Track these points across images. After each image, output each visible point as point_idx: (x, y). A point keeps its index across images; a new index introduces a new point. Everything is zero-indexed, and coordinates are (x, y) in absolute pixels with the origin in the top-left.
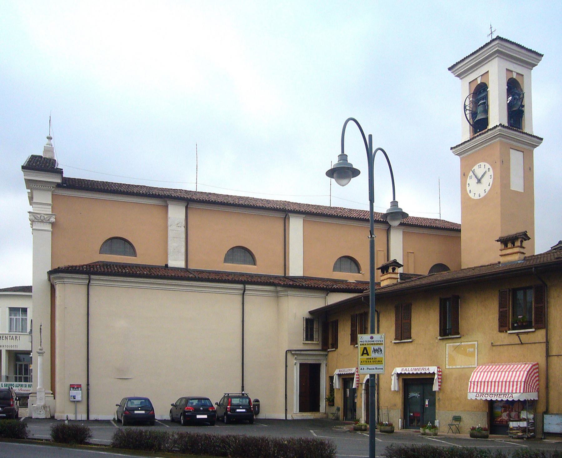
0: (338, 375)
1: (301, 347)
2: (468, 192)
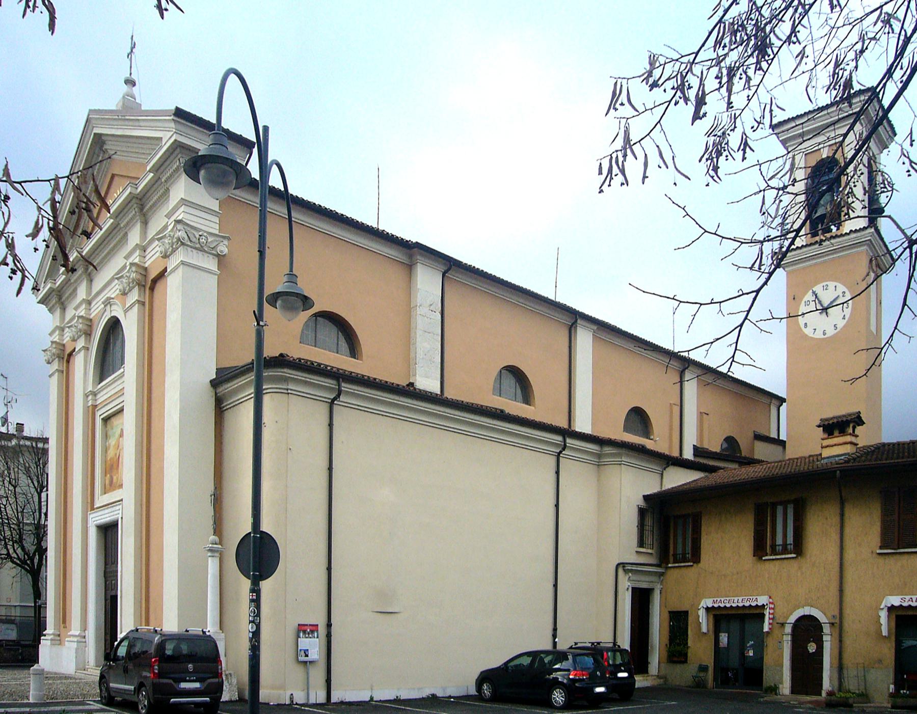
0: (706, 609)
1: (634, 559)
2: (802, 326)
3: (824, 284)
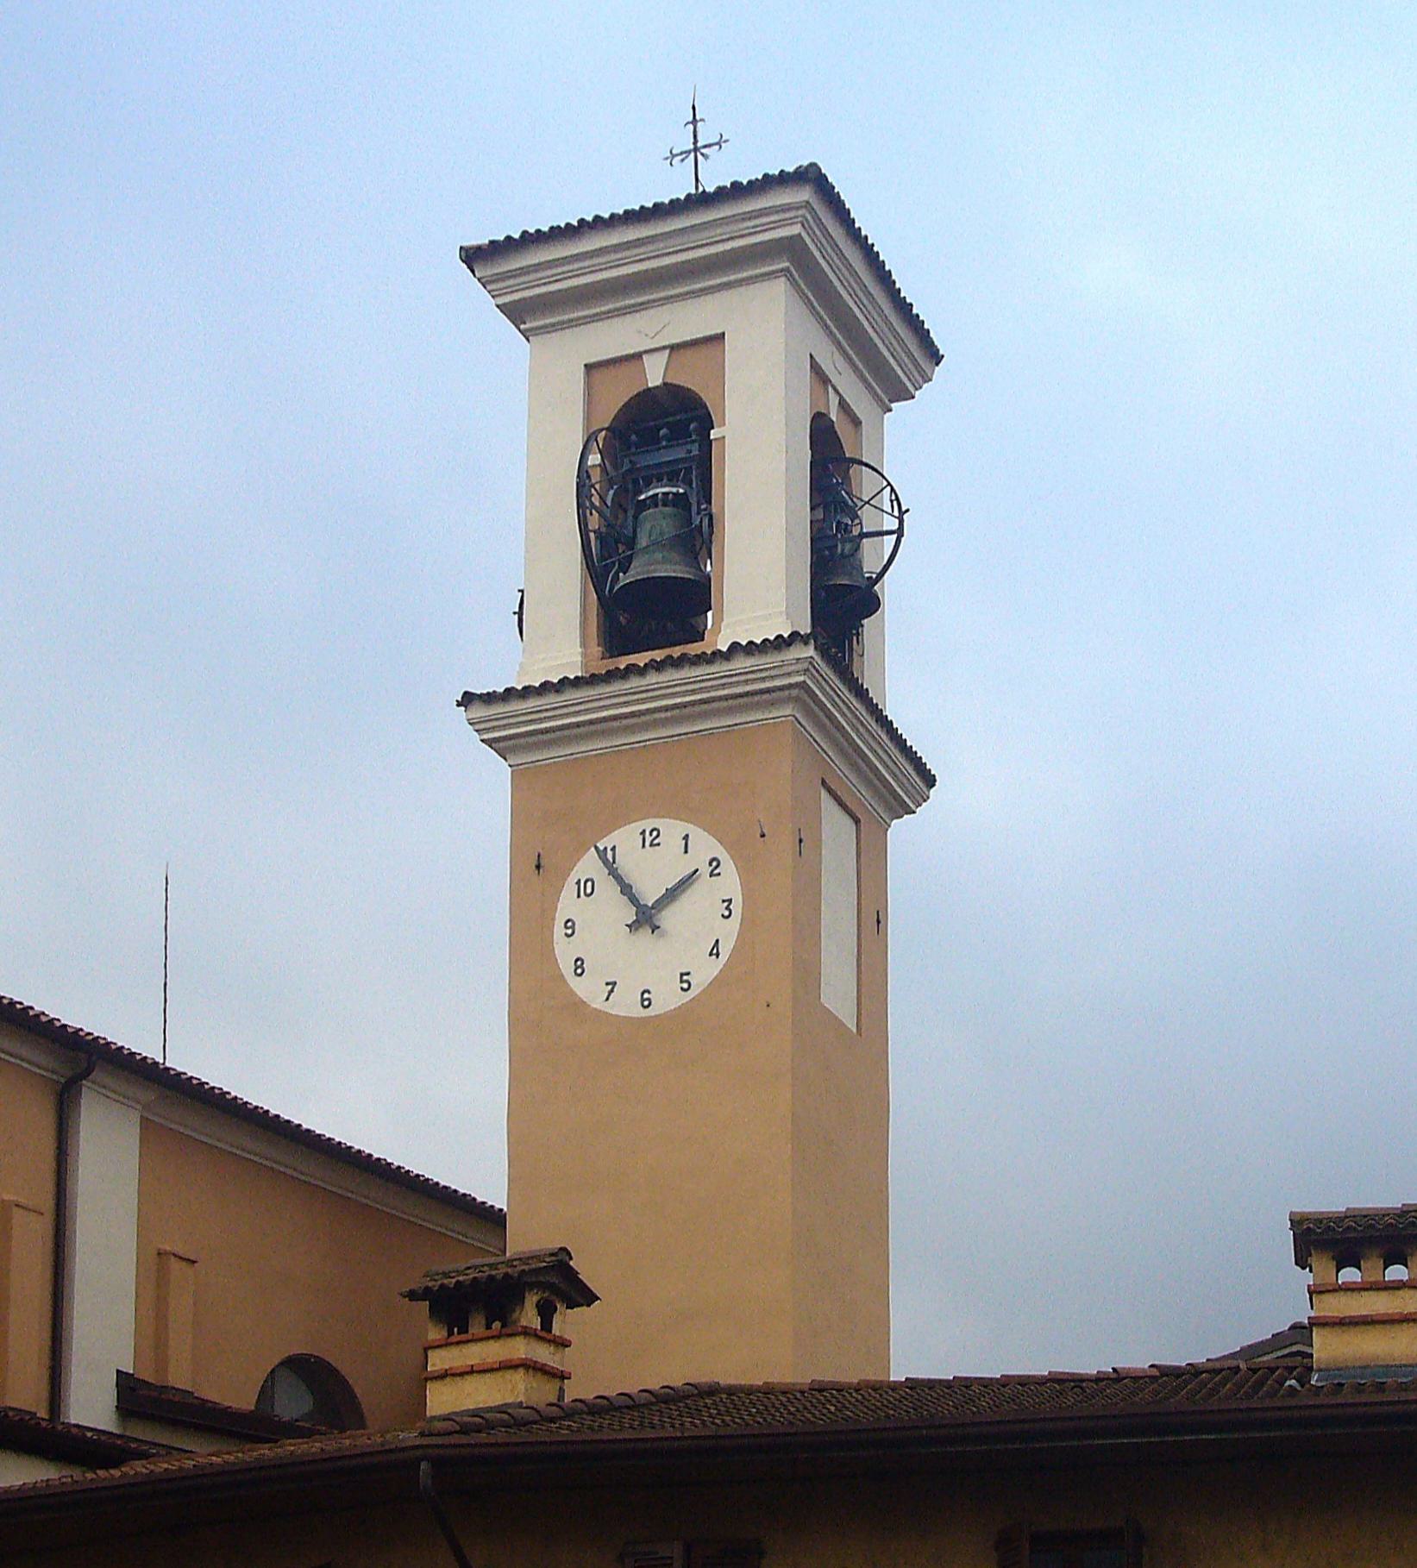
2: (567, 967)
3: (648, 824)
